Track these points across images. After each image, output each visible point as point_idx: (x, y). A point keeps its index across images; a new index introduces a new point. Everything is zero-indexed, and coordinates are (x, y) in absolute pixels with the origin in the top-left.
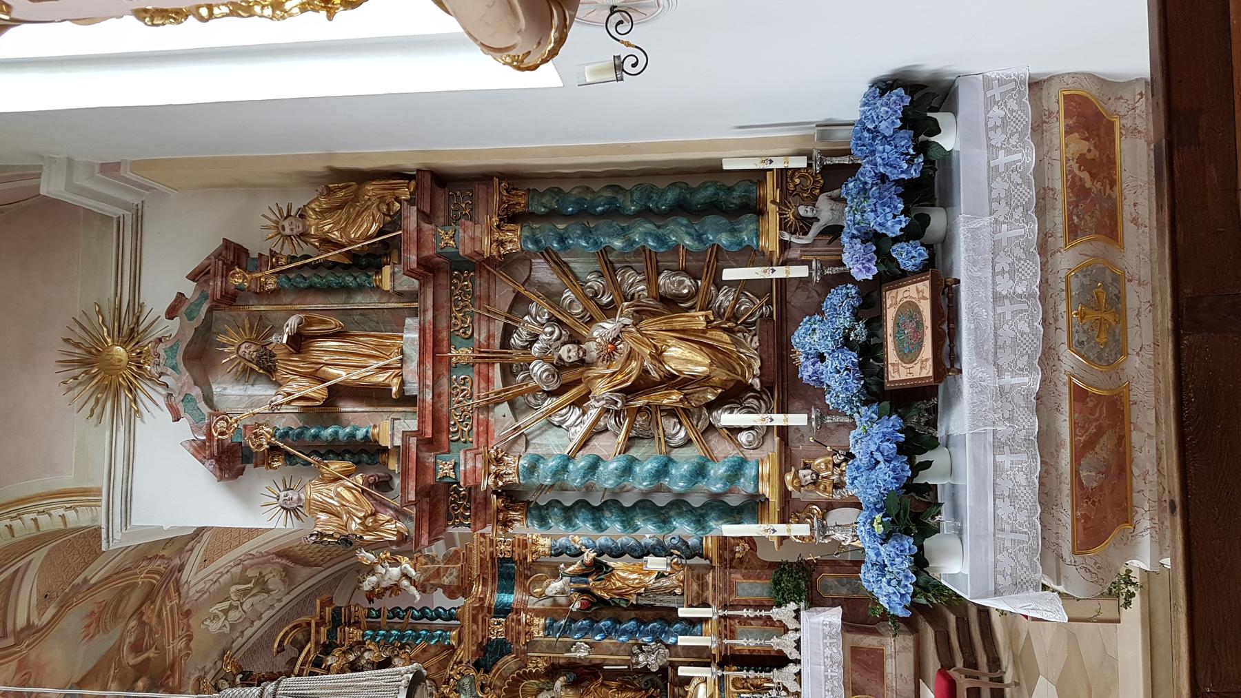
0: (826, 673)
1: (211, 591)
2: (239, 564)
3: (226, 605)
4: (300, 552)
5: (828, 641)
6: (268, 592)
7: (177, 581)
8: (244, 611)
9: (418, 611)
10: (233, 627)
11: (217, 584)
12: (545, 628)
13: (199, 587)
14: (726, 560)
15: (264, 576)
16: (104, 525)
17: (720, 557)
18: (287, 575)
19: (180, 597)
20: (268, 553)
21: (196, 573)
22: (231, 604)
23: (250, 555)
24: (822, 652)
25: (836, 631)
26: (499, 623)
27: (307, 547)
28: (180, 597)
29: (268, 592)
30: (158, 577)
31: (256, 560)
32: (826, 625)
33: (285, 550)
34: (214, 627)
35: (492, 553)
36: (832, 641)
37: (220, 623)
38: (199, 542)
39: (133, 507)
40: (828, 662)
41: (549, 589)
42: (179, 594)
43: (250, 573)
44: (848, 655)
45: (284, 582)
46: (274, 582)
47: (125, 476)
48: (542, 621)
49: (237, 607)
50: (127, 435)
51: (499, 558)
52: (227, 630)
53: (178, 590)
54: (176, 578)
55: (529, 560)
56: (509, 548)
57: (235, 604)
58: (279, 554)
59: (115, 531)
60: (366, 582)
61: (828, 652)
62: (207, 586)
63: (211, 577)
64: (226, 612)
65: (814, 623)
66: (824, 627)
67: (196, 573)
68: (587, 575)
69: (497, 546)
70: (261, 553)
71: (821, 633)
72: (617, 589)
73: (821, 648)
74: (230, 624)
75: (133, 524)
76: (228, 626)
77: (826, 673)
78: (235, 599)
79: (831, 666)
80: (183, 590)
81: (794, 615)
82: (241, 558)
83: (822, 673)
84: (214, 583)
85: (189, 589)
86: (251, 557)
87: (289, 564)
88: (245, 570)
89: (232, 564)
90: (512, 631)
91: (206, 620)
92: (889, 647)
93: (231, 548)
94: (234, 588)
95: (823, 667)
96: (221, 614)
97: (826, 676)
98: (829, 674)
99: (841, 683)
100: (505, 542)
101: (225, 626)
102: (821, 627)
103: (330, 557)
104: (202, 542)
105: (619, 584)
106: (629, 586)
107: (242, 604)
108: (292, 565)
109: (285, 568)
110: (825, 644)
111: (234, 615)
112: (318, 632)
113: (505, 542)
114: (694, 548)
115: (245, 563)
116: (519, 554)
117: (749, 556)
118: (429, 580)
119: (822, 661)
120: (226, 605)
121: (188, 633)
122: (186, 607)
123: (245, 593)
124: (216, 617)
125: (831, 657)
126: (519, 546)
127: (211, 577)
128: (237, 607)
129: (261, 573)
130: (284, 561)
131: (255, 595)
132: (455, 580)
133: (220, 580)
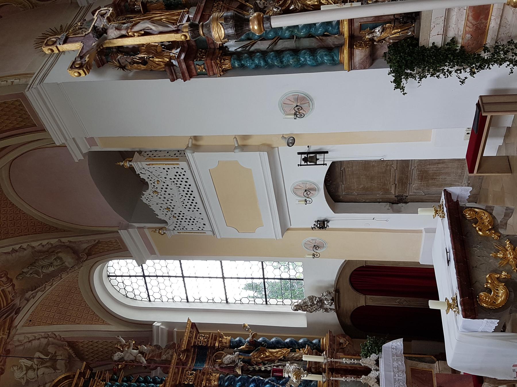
0: (395, 377)
1: (26, 347)
2: (46, 338)
3: (29, 363)
4: (82, 348)
5: (395, 358)
6: (55, 369)
7: (12, 320)
8: (37, 375)
9: (142, 378)
10: (28, 382)
11: (30, 344)
12: (219, 379)
13: (21, 338)
14: (334, 350)
15: (57, 356)
16: (30, 83)
17: (330, 346)
18: (70, 363)
19: (8, 336)
20: (64, 340)
21: (23, 326)
22: (32, 366)
23: (55, 334)
24: (391, 364)
25: (401, 353)
26: (191, 374)
27: (86, 346)
28: (8, 336)
29: (55, 369)
30: (5, 305)
31: (56, 341)
32: (394, 348)
33: (74, 343)
34: (18, 374)
35: (195, 342)
36: (397, 358)
37: (21, 375)
38: (34, 297)
39: (46, 78)
40: (396, 370)
41: (226, 358)
42: (9, 333)
43: (51, 349)
44: (409, 372)
45: (66, 366)
46: (61, 364)
47: (48, 69)
48: (218, 375)
49: (34, 370)
50: (55, 59)
51: (199, 346)
52: (23, 382)
53: (9, 329)
54: (12, 317)
55: (217, 345)
56: (206, 340)
57: (35, 366)
58: (72, 344)
59: (34, 84)
60: (117, 354)
61: (396, 364)
62: (25, 341)
63: (29, 335)
64: (28, 368)
65: (386, 347)
66: (393, 350)
67: (23, 326)
68: (249, 352)
69: (199, 338)
70: (60, 337)
71: (391, 353)
72: (267, 357)
73: (392, 363)
74: (27, 380)
75: (44, 82)
76: (25, 379)
77: (395, 377)
78: (36, 363)
79: (398, 372)
80: (12, 332)
81: (375, 362)
82: (49, 333)
83: (392, 377)
84: (30, 342)
85: (15, 334)
86: (54, 336)
87: (73, 354)
88: (48, 344)
89: (43, 334)
90: (198, 378)
91: (15, 365)
92: (435, 369)
93: (46, 324)
94: (38, 354)
95: (392, 373)
96: (24, 368)
97: (395, 379)
98: (397, 378)
99: (405, 383)
100: (204, 337)
101: (23, 378)
102: (390, 349)
103: (97, 359)
104: (36, 298)
105: (267, 354)
106: (274, 356)
107: (38, 369)
108: (74, 356)
109: (70, 357)
110: (394, 360)
111: (31, 374)
112: (79, 378)
113: (204, 337)
114: (315, 344)
115: (50, 339)
116: (211, 343)
117: (349, 348)
118: (154, 357)
119: (392, 370)
120: (29, 363)
121: (3, 367)
122: (9, 347)
123: (42, 362)
124: (21, 368)
125: (398, 368)
126: (212, 339)
127: (29, 335)
128: (34, 370)
129: (55, 353)
130: (70, 351)
131: (46, 367)
132: (170, 356)
133: (33, 342)
